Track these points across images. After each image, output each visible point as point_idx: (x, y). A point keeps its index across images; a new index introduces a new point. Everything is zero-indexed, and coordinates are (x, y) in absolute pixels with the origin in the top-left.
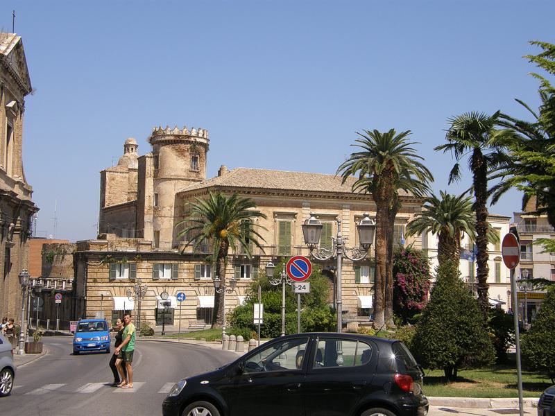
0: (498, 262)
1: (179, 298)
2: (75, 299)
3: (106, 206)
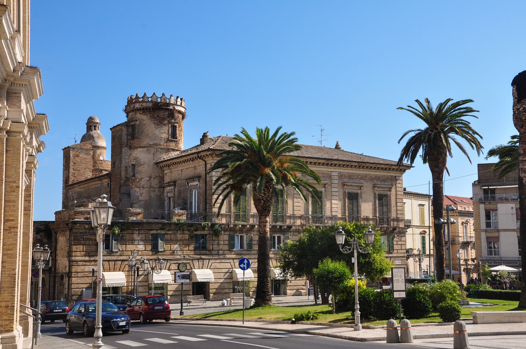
0: (423, 235)
1: (242, 266)
2: (55, 277)
3: (70, 183)
